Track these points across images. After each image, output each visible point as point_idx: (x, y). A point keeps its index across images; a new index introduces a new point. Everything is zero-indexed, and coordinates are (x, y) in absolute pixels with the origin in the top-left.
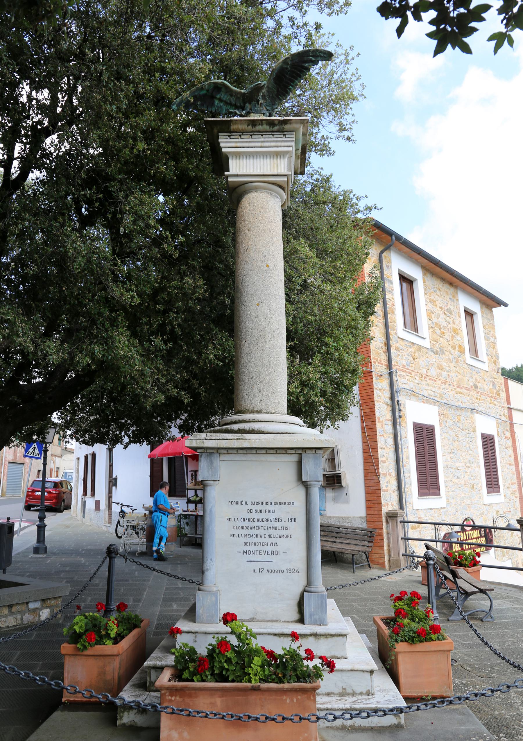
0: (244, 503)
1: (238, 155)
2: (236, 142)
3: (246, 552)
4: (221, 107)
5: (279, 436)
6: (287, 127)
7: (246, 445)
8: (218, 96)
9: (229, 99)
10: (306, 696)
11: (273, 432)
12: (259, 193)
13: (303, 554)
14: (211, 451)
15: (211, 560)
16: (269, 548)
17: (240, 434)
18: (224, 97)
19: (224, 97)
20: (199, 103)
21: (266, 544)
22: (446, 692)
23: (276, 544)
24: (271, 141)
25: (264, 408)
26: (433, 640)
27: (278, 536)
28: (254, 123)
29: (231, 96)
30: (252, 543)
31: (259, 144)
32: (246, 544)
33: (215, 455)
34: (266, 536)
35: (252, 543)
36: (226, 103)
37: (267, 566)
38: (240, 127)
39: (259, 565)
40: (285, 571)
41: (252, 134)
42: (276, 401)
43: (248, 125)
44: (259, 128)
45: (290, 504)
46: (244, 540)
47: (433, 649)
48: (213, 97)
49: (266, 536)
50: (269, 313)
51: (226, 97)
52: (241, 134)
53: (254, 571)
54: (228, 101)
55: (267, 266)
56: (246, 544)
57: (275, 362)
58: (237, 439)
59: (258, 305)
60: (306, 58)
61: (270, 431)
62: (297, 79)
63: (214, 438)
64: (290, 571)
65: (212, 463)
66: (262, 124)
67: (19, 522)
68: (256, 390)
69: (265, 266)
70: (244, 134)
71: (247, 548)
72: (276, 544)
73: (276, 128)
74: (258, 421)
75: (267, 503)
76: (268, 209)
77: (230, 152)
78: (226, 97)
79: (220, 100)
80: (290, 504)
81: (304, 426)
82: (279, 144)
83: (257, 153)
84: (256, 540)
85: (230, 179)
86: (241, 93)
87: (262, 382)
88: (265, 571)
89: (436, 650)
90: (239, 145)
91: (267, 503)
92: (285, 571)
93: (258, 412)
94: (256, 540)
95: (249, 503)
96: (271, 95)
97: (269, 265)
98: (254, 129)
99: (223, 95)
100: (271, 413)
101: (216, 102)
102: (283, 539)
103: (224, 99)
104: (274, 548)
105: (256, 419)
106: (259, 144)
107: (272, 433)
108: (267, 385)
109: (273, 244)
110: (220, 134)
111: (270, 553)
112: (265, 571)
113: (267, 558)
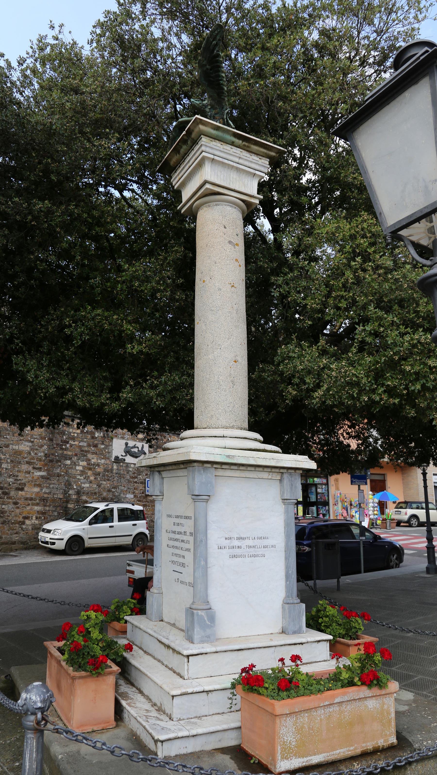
42: (209, 415)
50: (205, 328)
55: (204, 281)
57: (208, 376)
97: (205, 280)
109: (209, 257)
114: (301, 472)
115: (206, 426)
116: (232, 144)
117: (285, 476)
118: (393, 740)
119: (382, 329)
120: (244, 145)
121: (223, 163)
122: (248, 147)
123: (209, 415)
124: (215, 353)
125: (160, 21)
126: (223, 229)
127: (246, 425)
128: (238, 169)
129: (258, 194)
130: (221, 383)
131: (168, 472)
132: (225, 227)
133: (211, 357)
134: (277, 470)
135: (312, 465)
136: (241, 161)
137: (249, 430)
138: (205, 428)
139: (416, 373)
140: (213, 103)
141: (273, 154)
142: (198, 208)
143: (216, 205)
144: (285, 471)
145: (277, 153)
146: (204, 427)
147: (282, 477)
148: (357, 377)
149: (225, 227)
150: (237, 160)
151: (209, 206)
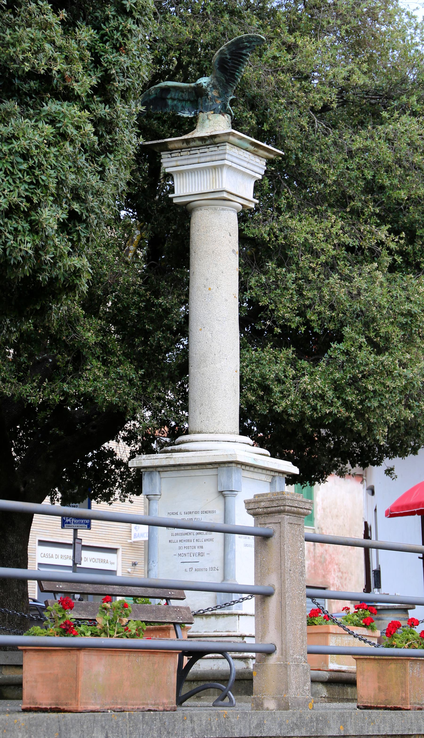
0: (179, 513)
1: (180, 173)
2: (176, 161)
3: (180, 555)
4: (176, 105)
5: (198, 454)
6: (217, 140)
7: (172, 462)
8: (169, 97)
9: (182, 96)
10: (164, 633)
11: (196, 450)
12: (203, 211)
13: (221, 554)
14: (151, 470)
15: (153, 561)
16: (197, 551)
17: (170, 454)
18: (175, 95)
19: (175, 95)
20: (151, 107)
21: (195, 547)
22: (323, 667)
23: (202, 547)
24: (206, 156)
25: (204, 429)
26: (316, 625)
27: (203, 540)
28: (187, 141)
29: (183, 92)
30: (185, 547)
31: (196, 161)
32: (180, 548)
33: (154, 473)
34: (195, 540)
35: (185, 547)
36: (179, 100)
37: (195, 566)
38: (177, 145)
39: (189, 565)
40: (208, 569)
41: (189, 149)
42: (216, 421)
43: (183, 143)
44: (192, 144)
45: (213, 512)
46: (179, 544)
47: (313, 632)
48: (164, 99)
49: (195, 540)
50: (211, 337)
51: (177, 94)
52: (180, 151)
53: (186, 570)
54: (181, 98)
55: (210, 289)
56: (180, 548)
57: (215, 384)
58: (166, 458)
59: (201, 330)
60: (241, 45)
61: (194, 450)
62: (240, 65)
63: (153, 458)
64: (212, 569)
65: (152, 480)
66: (194, 141)
67: (85, 554)
68: (198, 412)
69: (207, 289)
70: (183, 150)
71: (181, 552)
72: (202, 547)
73: (208, 142)
74: (192, 441)
75: (196, 513)
76: (212, 227)
77: (172, 172)
78: (177, 94)
79: (173, 99)
80: (213, 512)
81: (253, 446)
82: (214, 158)
83: (196, 169)
84: (187, 544)
85: (175, 201)
86: (191, 87)
87: (202, 404)
88: (194, 570)
89: (316, 632)
90: (179, 163)
91: (196, 513)
92: (208, 569)
93: (199, 433)
94: (187, 544)
95: (183, 513)
96: (221, 84)
97: (212, 288)
98: (189, 146)
99: (173, 94)
100: (210, 433)
101: (170, 102)
102: (207, 542)
103: (176, 97)
104: (200, 550)
105: (191, 440)
106: (196, 161)
107: (195, 451)
108: (207, 407)
109: (216, 265)
110: (162, 153)
111: (197, 554)
112: (194, 570)
113: (195, 559)
114: (285, 476)
115: (213, 431)
116: (246, 150)
117: (277, 479)
118: (409, 611)
119: (353, 349)
120: (254, 151)
121: (236, 169)
122: (257, 152)
123: (216, 421)
124: (222, 362)
125: (290, 152)
126: (229, 237)
127: (237, 430)
128: (244, 173)
129: (254, 197)
130: (228, 392)
131: (251, 473)
132: (230, 235)
133: (218, 366)
134: (268, 472)
135: (296, 470)
136: (248, 166)
137: (241, 434)
138: (212, 433)
139: (374, 392)
140: (216, 83)
141: (272, 156)
142: (200, 206)
143: (223, 209)
144: (277, 474)
145: (275, 155)
146: (211, 431)
147: (272, 480)
148: (322, 390)
149: (230, 235)
150: (245, 164)
151: (216, 209)
